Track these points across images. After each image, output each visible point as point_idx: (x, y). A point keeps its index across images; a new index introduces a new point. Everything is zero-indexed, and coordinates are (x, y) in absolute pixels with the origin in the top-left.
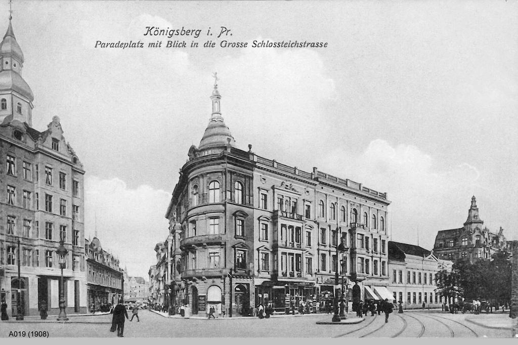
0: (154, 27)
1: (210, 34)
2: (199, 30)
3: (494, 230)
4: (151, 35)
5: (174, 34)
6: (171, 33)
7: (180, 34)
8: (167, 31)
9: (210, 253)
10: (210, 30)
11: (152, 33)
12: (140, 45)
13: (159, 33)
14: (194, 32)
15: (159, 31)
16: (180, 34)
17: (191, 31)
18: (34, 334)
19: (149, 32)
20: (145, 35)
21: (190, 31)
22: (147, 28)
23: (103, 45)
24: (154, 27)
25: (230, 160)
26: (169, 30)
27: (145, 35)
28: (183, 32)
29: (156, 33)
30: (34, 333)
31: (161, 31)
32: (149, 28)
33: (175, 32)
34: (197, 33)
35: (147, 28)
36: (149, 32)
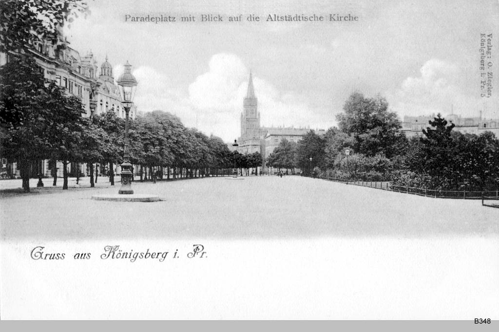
1: (176, 256)
8: (131, 254)
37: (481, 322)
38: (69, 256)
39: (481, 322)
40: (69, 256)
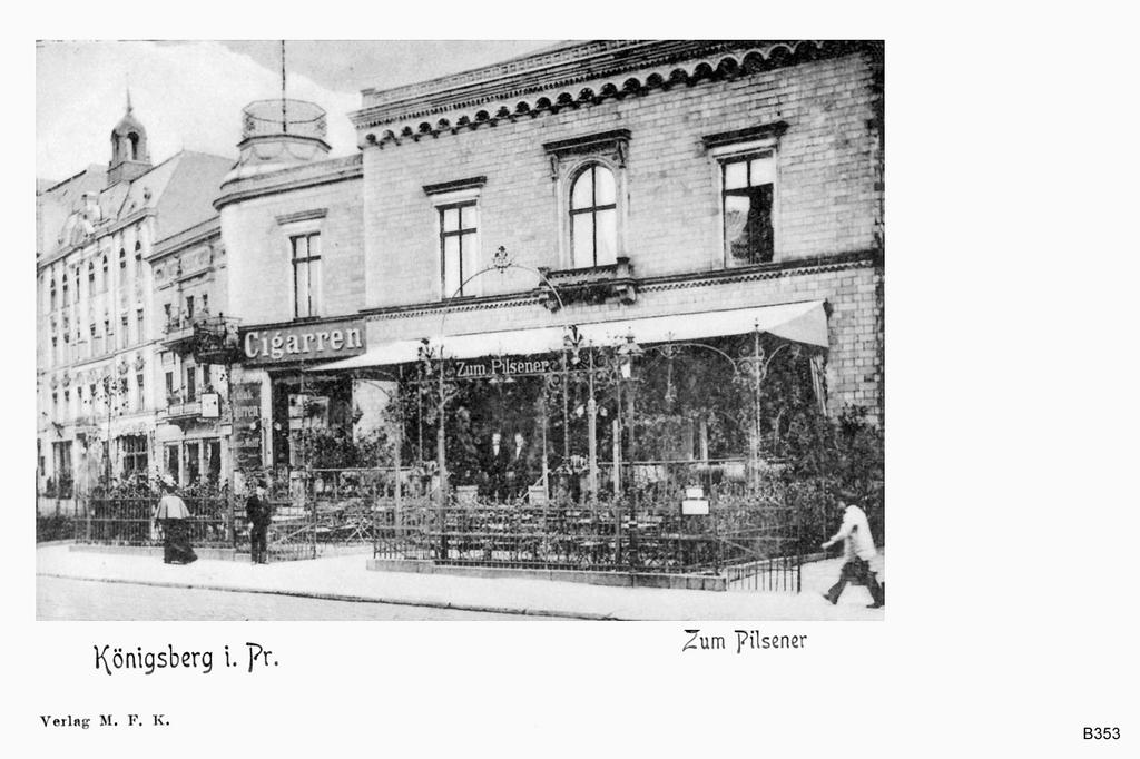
1: (231, 664)
37: (1098, 736)
39: (1098, 736)
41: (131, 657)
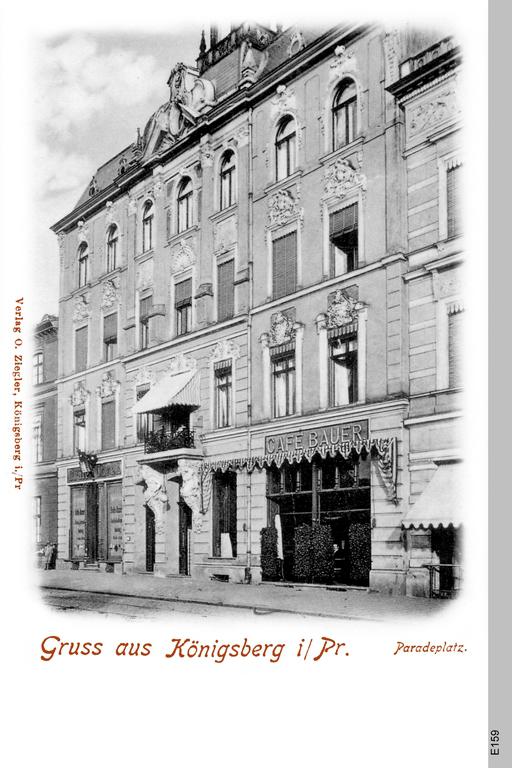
0: (188, 640)
2: (123, 644)
3: (456, 405)
4: (182, 656)
5: (227, 654)
6: (222, 653)
7: (240, 653)
9: (247, 280)
10: (303, 643)
11: (184, 652)
12: (457, 648)
13: (217, 649)
14: (270, 649)
15: (199, 649)
16: (240, 653)
17: (264, 648)
18: (496, 742)
19: (178, 651)
20: (168, 656)
21: (261, 646)
22: (174, 640)
23: (407, 649)
24: (188, 640)
25: (394, 89)
26: (218, 646)
27: (168, 656)
28: (246, 649)
29: (192, 651)
30: (493, 742)
31: (202, 648)
32: (179, 641)
33: (230, 650)
34: (277, 652)
35: (174, 640)
36: (178, 651)
38: (108, 649)
40: (108, 649)
41: (133, 652)
